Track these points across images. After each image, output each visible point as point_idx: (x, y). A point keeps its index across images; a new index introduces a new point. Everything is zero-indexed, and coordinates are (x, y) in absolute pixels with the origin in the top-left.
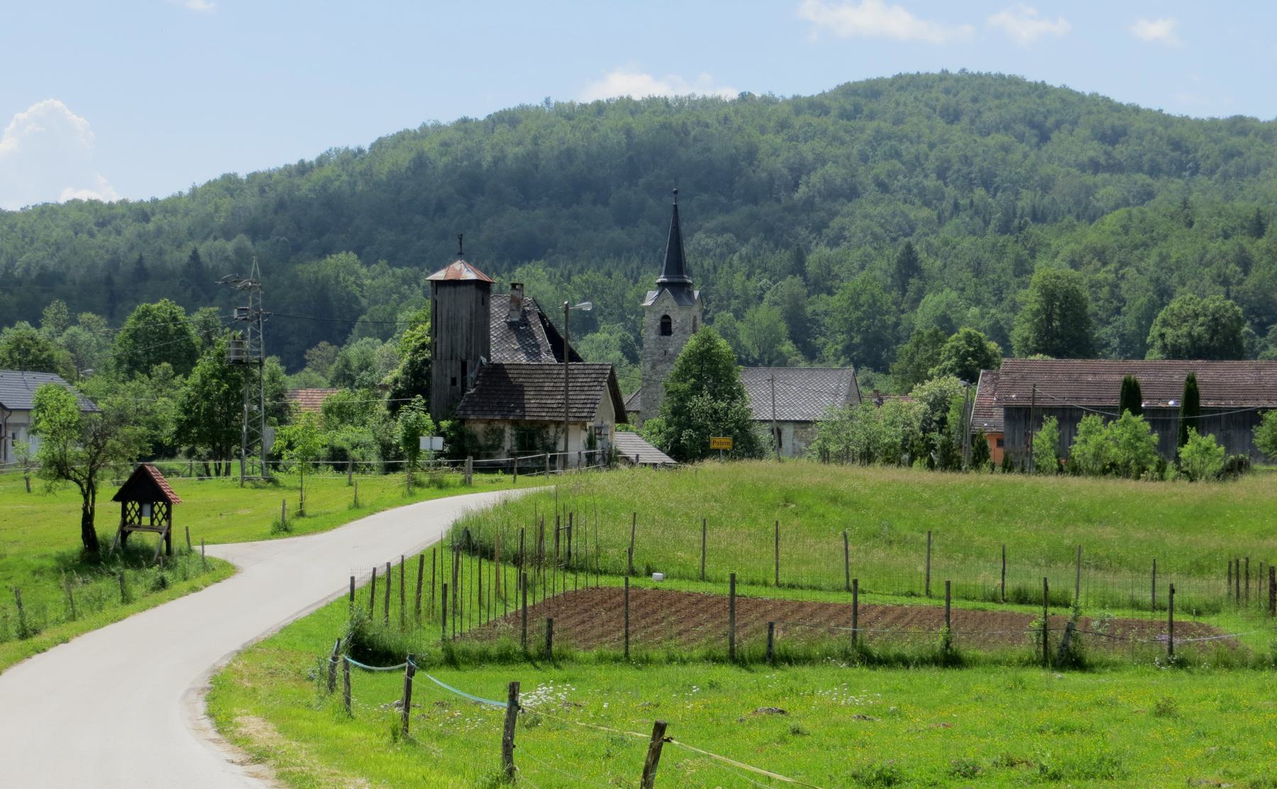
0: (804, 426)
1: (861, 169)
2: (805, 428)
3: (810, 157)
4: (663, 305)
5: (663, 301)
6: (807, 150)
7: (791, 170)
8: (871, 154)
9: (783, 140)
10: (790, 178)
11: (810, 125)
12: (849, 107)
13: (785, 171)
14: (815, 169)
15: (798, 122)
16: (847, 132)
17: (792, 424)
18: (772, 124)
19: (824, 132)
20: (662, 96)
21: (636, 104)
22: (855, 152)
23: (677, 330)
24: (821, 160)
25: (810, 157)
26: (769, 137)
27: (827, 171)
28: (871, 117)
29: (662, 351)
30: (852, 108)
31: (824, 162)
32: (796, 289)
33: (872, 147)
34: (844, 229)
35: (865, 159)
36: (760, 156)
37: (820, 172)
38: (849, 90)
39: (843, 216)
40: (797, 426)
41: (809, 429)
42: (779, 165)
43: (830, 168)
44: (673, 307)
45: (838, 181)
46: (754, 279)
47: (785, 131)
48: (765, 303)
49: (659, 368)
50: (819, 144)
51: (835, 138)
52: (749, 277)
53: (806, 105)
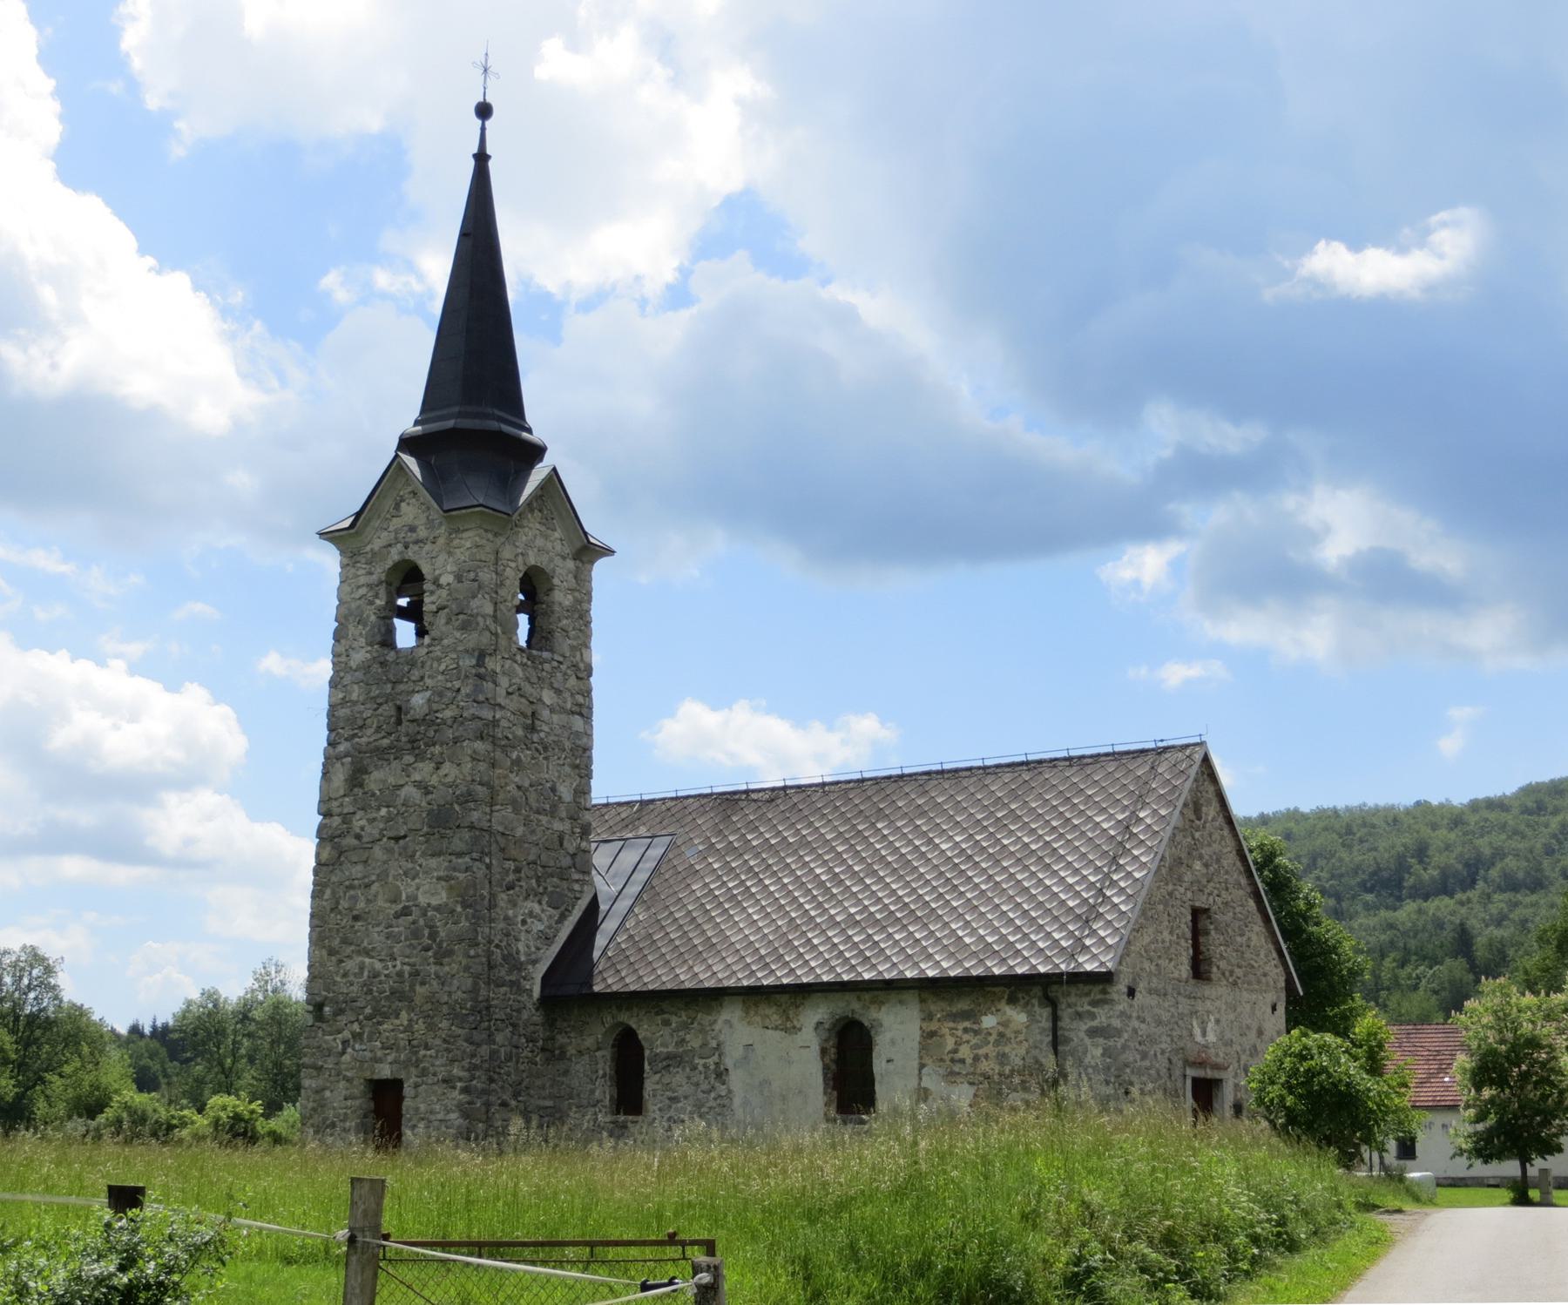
0: (963, 1005)
1: (1546, 863)
2: (965, 1015)
3: (1487, 851)
4: (396, 523)
5: (397, 507)
6: (1484, 845)
7: (1467, 865)
8: (1557, 847)
9: (1457, 836)
10: (1465, 873)
11: (1486, 820)
12: (1530, 804)
13: (1460, 867)
14: (1493, 864)
15: (1473, 819)
16: (1528, 826)
17: (911, 997)
18: (1446, 821)
19: (1503, 827)
20: (1331, 806)
21: (1303, 815)
22: (1539, 846)
23: (442, 619)
24: (1499, 854)
25: (1487, 851)
26: (1442, 833)
27: (1507, 865)
28: (1556, 812)
29: (388, 710)
30: (1535, 805)
31: (1503, 856)
32: (1458, 974)
33: (1558, 840)
34: (1527, 921)
35: (1549, 852)
36: (1430, 853)
37: (1499, 866)
38: (1529, 790)
39: (1526, 907)
40: (938, 1007)
41: (989, 1021)
42: (1452, 861)
43: (1510, 863)
44: (430, 524)
45: (1521, 875)
46: (1408, 969)
47: (1459, 828)
48: (1421, 992)
49: (377, 778)
50: (1499, 839)
51: (1516, 832)
52: (1402, 965)
53: (1484, 804)
